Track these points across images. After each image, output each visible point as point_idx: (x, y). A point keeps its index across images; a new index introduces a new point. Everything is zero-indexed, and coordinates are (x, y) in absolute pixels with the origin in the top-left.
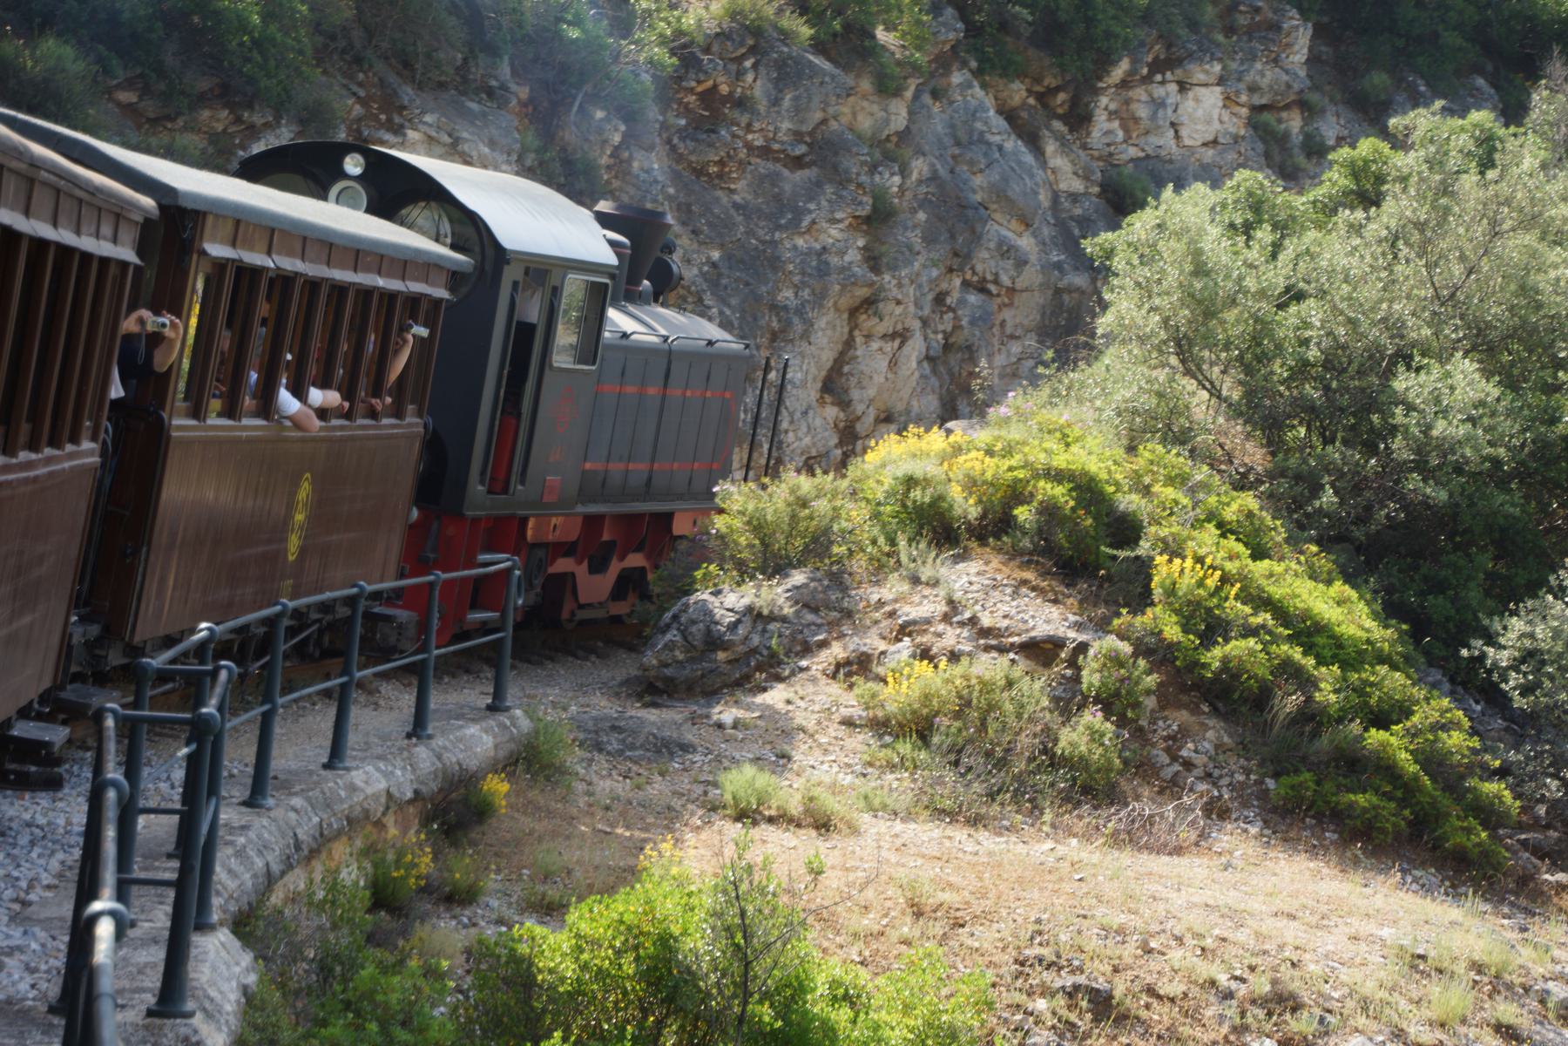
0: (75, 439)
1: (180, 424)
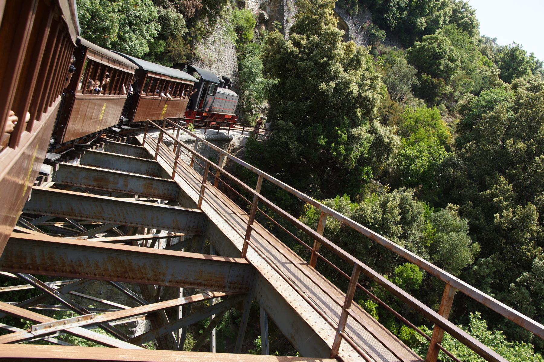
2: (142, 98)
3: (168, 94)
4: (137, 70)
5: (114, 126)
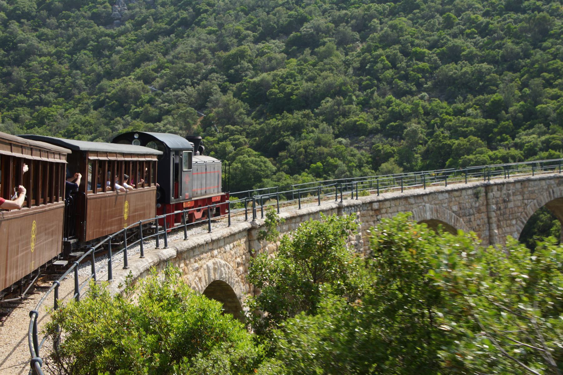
0: (57, 200)
1: (90, 194)
2: (90, 199)
3: (125, 184)
4: (69, 157)
5: (56, 258)
